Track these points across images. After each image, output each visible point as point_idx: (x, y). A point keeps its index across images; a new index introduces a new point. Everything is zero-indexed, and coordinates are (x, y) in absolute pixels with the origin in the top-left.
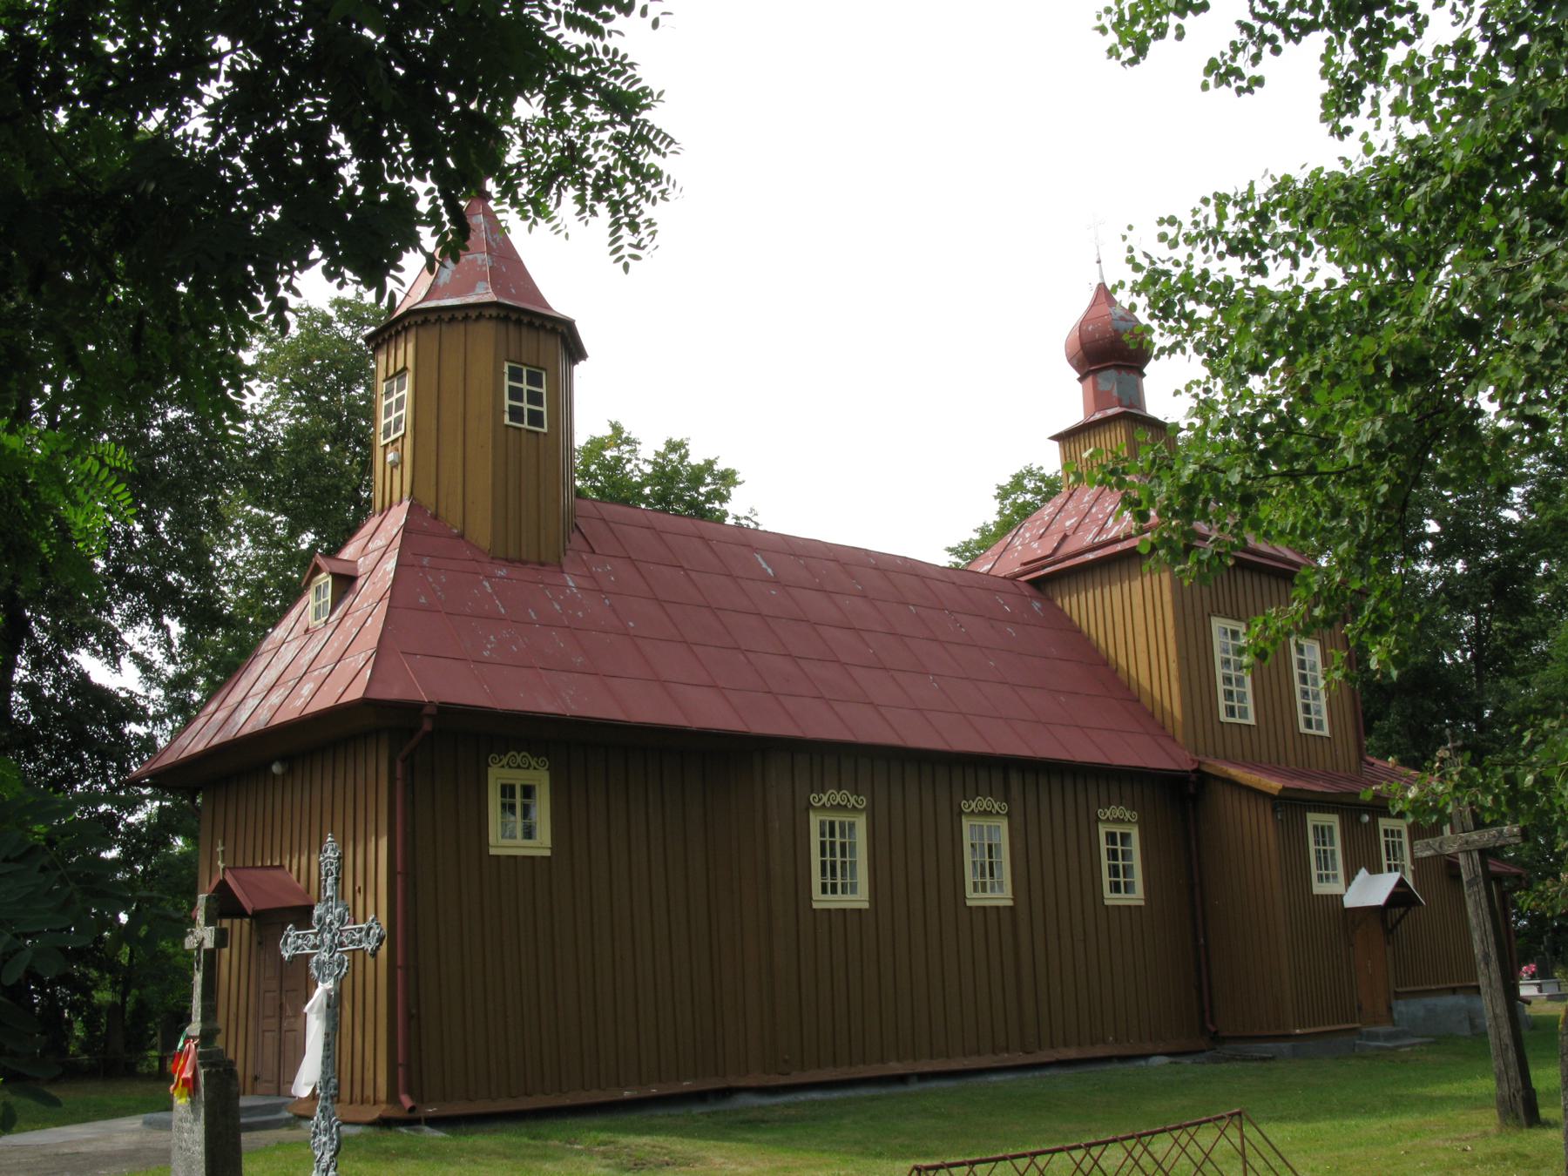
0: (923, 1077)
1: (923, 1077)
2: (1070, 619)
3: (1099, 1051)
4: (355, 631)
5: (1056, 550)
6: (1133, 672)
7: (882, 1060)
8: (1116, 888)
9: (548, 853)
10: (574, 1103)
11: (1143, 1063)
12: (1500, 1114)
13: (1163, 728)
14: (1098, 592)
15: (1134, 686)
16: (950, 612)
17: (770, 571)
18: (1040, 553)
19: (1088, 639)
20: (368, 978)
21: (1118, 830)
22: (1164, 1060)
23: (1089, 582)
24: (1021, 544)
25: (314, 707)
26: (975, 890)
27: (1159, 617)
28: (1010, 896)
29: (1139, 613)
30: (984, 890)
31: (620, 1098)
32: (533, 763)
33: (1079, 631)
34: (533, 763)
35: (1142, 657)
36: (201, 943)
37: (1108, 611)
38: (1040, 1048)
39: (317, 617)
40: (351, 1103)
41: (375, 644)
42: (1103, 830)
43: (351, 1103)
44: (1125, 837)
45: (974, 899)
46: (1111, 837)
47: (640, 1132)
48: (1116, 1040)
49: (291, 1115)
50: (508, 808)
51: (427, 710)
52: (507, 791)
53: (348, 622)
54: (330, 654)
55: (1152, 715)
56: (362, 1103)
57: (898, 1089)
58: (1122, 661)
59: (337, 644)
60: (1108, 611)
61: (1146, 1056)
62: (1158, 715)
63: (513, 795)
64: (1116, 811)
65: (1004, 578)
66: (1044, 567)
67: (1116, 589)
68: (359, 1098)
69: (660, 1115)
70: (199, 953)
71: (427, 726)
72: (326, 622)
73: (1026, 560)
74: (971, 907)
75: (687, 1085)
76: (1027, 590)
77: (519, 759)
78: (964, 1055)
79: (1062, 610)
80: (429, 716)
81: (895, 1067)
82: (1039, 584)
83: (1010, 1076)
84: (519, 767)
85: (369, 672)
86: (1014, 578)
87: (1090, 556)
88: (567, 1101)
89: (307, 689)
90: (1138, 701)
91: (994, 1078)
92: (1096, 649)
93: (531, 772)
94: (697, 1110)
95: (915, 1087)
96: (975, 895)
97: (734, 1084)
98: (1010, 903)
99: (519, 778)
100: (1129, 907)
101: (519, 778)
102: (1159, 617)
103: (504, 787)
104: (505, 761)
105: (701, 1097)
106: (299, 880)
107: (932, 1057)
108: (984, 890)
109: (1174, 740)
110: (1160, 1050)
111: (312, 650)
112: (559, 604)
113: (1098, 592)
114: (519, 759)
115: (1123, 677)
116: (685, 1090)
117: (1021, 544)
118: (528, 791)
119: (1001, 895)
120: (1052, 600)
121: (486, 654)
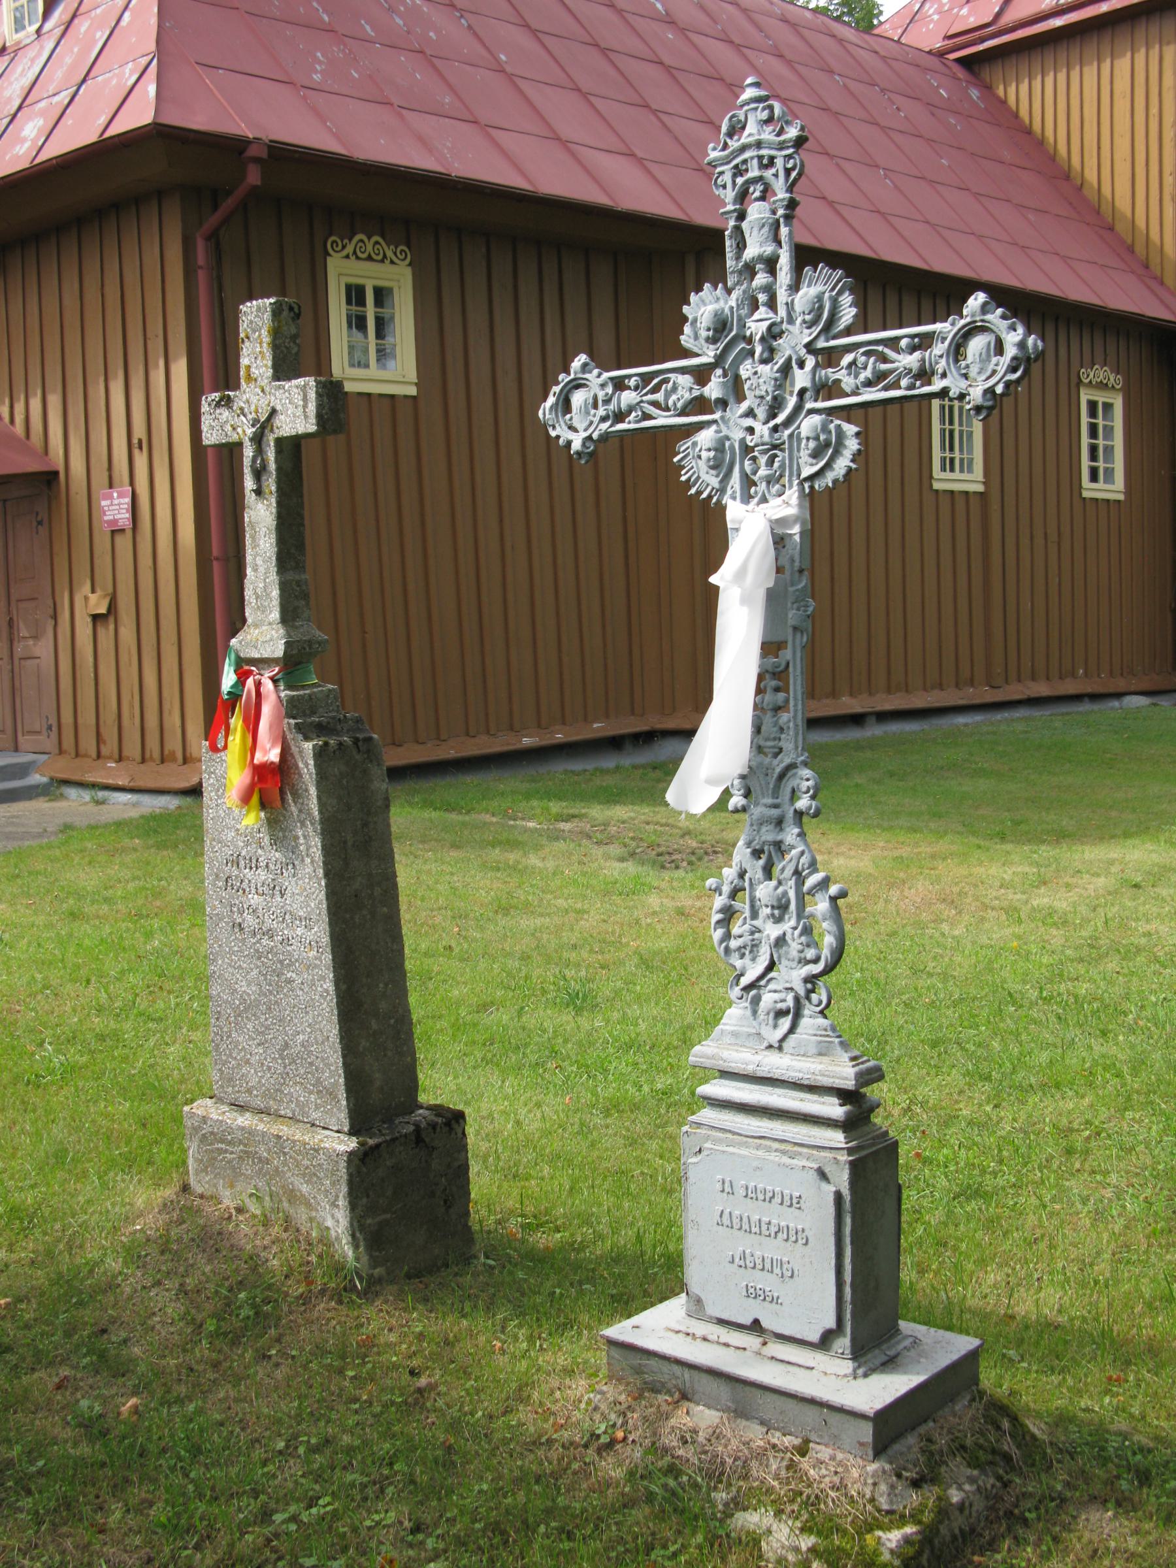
0: (883, 717)
1: (883, 717)
2: (1016, 115)
3: (1070, 687)
4: (101, 36)
5: (998, 16)
6: (1106, 190)
7: (834, 694)
8: (1094, 477)
9: (412, 391)
10: (459, 755)
11: (1116, 704)
12: (582, 801)
13: (1147, 267)
14: (1062, 76)
15: (1106, 209)
16: (882, 90)
17: (659, 6)
18: (973, 22)
19: (1041, 143)
20: (120, 577)
21: (1101, 398)
22: (1142, 701)
23: (1049, 61)
24: (938, 12)
25: (59, 146)
26: (943, 469)
27: (1154, 110)
28: (981, 478)
29: (1123, 106)
30: (952, 470)
31: (518, 746)
32: (390, 254)
33: (1029, 132)
34: (390, 254)
35: (1123, 169)
36: (263, 427)
37: (1075, 103)
38: (1007, 682)
39: (19, 25)
40: (143, 760)
41: (152, 46)
42: (1085, 396)
43: (143, 760)
44: (1108, 407)
45: (943, 480)
46: (1092, 406)
47: (612, 797)
48: (1086, 674)
49: (45, 780)
50: (358, 323)
51: (252, 151)
52: (355, 294)
53: (82, 26)
54: (58, 74)
55: (1131, 249)
56: (163, 761)
57: (852, 734)
58: (1091, 176)
59: (71, 58)
60: (1075, 103)
61: (1119, 695)
62: (1140, 249)
63: (361, 302)
64: (1099, 373)
65: (930, 52)
66: (983, 40)
67: (1090, 72)
68: (156, 754)
69: (560, 768)
70: (259, 450)
71: (254, 177)
72: (38, 32)
73: (951, 33)
74: (937, 491)
75: (599, 728)
76: (961, 73)
77: (369, 248)
78: (925, 689)
79: (1004, 102)
80: (257, 160)
81: (853, 705)
82: (967, 63)
83: (978, 718)
84: (370, 258)
85: (152, 89)
86: (941, 54)
87: (1058, 22)
88: (450, 752)
89: (31, 129)
90: (1111, 229)
91: (961, 720)
92: (1053, 158)
93: (386, 268)
94: (609, 761)
95: (874, 731)
96: (943, 475)
97: (659, 726)
98: (980, 488)
99: (370, 275)
100: (1108, 501)
101: (370, 275)
102: (1154, 110)
103: (349, 288)
104: (349, 249)
105: (615, 743)
106: (12, 421)
107: (889, 691)
108: (952, 470)
109: (1162, 283)
110: (1133, 688)
111: (23, 74)
112: (401, 17)
113: (1062, 76)
114: (369, 248)
115: (1092, 196)
116: (557, 741)
117: (938, 12)
118: (382, 295)
119: (971, 480)
120: (988, 88)
121: (317, 77)
